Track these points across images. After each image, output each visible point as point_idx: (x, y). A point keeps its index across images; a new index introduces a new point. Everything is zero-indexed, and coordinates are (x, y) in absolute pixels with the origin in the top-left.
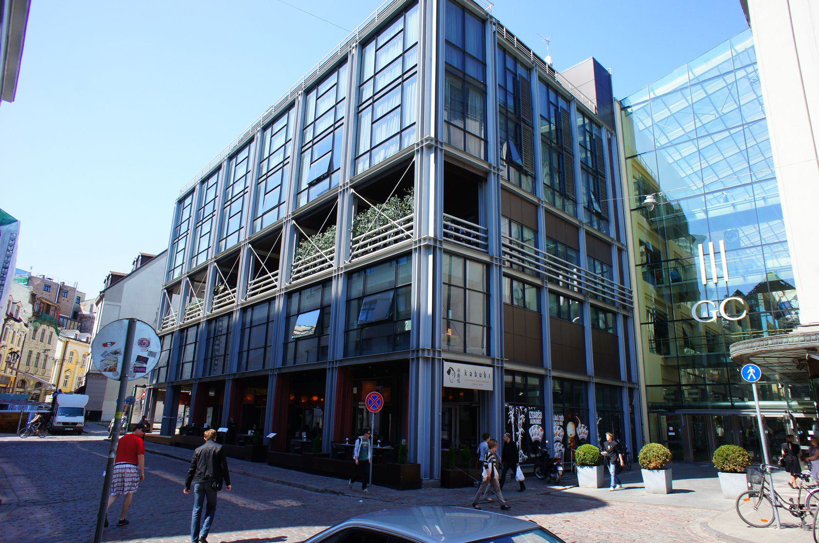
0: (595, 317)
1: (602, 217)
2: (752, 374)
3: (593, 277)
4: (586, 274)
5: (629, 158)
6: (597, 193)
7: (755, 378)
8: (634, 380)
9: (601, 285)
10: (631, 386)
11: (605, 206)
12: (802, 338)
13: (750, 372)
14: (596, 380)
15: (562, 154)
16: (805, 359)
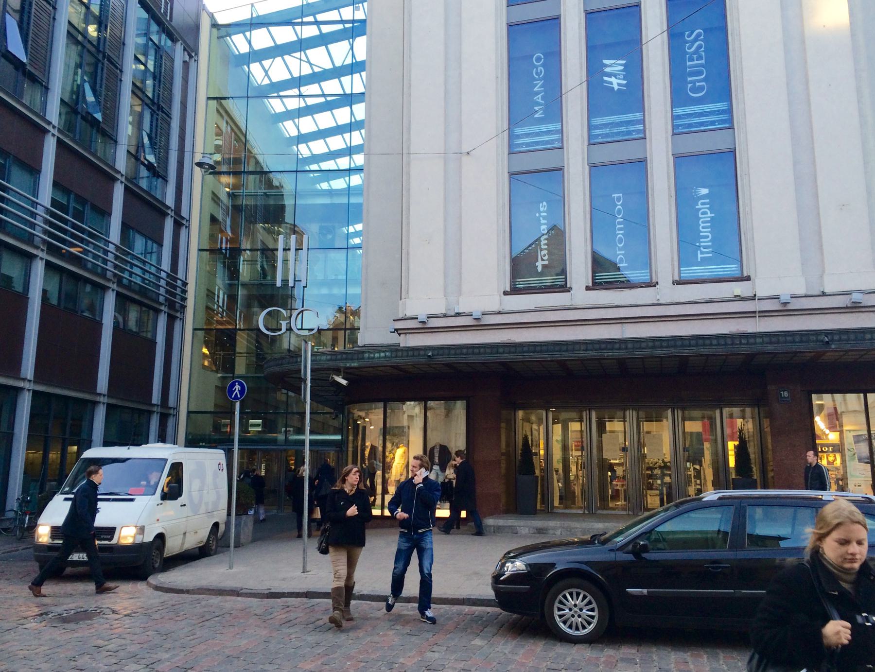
0: (844, 457)
1: (157, 173)
2: (237, 391)
3: (102, 250)
4: (117, 247)
5: (214, 98)
6: (153, 135)
7: (239, 396)
8: (172, 403)
9: (141, 268)
10: (165, 411)
11: (164, 160)
12: (329, 357)
13: (235, 389)
14: (32, 386)
15: (103, 64)
16: (329, 380)
